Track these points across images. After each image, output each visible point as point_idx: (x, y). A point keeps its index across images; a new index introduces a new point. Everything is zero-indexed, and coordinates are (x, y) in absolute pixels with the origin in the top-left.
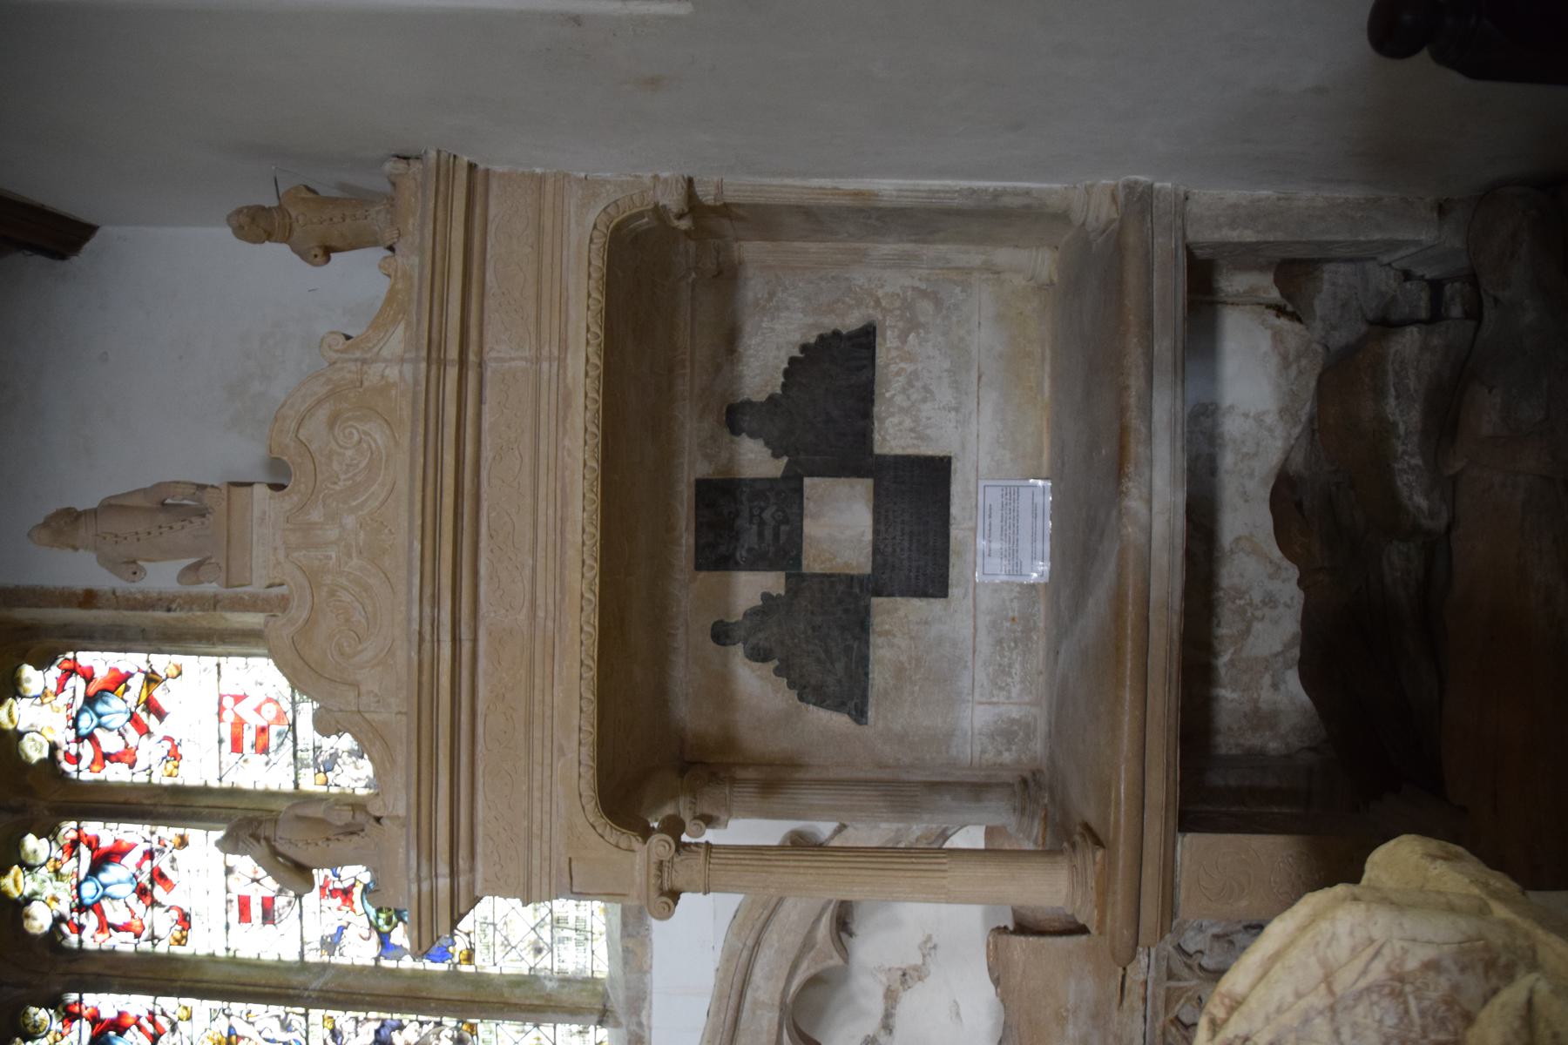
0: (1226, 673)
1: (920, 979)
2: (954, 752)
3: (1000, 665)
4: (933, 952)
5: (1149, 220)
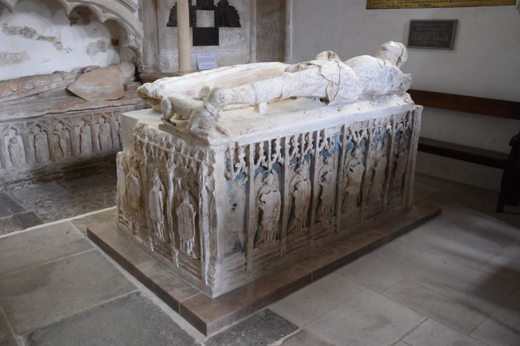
1: (57, 48)
2: (162, 49)
4: (67, 52)
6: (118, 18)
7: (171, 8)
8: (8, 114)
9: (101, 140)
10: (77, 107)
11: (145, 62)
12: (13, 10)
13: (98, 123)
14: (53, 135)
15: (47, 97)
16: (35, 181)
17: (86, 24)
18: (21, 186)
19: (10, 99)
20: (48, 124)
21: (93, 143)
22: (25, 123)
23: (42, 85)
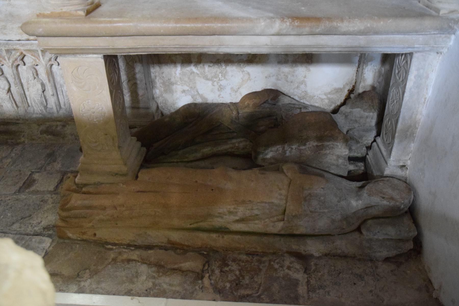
0: (188, 70)
5: (435, 32)
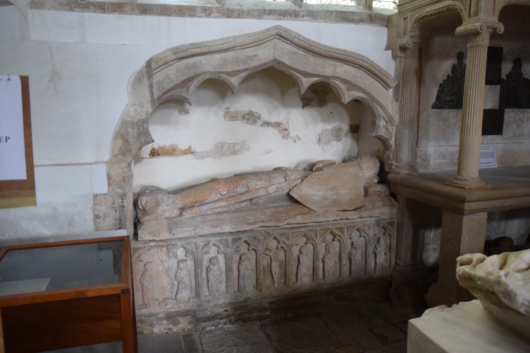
1: (283, 136)
3: (445, 155)
6: (366, 97)
7: (441, 83)
8: (212, 226)
9: (326, 266)
10: (299, 219)
11: (396, 158)
12: (235, 91)
13: (324, 242)
14: (264, 255)
15: (262, 204)
16: (233, 321)
17: (321, 106)
18: (214, 325)
19: (217, 206)
20: (259, 241)
21: (314, 269)
22: (230, 238)
23: (258, 187)
